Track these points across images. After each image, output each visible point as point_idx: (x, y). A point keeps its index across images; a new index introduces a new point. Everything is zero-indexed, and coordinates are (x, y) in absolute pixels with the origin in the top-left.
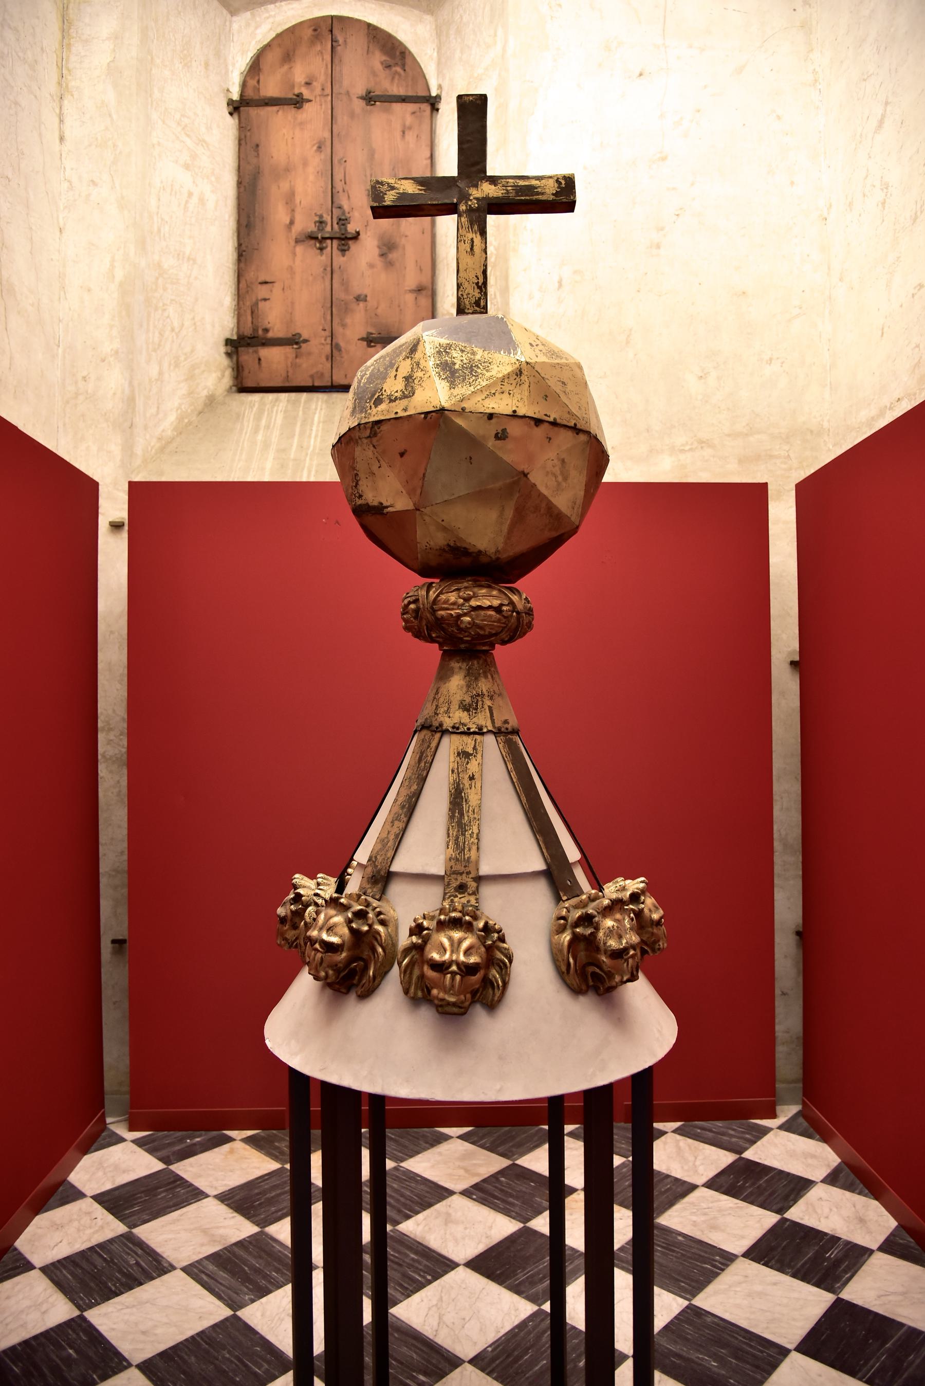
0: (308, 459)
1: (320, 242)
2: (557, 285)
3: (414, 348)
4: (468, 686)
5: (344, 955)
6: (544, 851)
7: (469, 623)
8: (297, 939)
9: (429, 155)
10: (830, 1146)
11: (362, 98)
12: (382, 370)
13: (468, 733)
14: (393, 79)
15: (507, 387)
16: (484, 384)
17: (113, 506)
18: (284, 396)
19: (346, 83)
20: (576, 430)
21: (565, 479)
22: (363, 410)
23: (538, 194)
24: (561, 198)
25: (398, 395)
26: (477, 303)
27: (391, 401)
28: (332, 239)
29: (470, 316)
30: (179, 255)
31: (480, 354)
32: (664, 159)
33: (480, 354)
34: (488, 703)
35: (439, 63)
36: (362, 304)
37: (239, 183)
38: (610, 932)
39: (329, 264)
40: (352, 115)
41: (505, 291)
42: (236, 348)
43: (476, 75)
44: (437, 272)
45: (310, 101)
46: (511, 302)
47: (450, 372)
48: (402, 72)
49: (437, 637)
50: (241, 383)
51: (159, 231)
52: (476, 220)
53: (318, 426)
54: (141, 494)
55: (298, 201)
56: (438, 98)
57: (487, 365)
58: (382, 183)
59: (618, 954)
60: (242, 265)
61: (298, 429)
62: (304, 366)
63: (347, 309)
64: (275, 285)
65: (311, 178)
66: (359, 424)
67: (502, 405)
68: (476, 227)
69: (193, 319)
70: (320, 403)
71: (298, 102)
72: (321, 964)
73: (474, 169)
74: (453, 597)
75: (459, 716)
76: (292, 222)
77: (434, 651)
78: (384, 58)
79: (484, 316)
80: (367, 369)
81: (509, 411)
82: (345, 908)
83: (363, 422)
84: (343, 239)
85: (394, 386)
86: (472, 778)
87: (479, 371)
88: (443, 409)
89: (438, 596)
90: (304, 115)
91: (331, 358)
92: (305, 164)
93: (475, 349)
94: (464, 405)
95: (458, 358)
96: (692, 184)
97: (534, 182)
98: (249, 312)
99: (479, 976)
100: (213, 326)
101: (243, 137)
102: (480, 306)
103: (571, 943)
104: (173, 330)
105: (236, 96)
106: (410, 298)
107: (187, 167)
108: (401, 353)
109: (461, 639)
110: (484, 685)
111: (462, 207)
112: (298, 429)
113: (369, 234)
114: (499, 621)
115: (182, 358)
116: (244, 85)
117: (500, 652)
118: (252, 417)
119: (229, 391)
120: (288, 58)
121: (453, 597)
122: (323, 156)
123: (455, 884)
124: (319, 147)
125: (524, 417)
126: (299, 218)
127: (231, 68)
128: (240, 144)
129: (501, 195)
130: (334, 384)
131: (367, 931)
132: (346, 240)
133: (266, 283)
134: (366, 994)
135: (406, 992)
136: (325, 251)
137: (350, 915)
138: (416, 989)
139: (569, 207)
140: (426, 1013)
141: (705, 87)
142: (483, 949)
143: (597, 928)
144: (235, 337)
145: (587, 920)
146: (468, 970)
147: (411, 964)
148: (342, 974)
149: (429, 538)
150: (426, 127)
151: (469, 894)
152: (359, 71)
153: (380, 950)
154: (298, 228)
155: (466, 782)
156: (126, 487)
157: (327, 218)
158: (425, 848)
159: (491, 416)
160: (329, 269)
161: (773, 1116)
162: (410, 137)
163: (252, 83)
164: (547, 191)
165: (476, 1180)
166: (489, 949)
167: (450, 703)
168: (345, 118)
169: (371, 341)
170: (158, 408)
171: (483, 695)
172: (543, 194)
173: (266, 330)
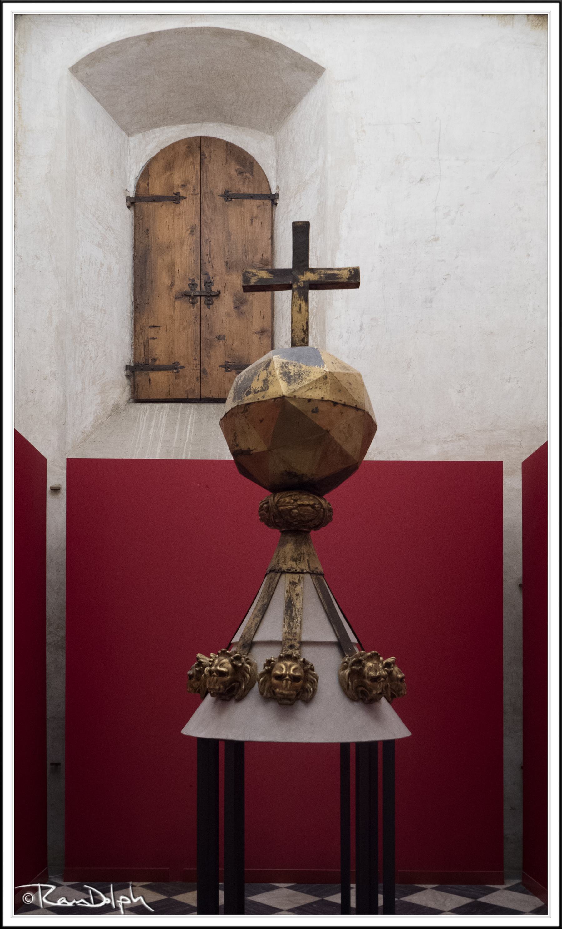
0: (185, 447)
1: (193, 298)
2: (359, 328)
3: (268, 364)
4: (296, 549)
5: (229, 677)
6: (337, 632)
7: (297, 513)
8: (199, 687)
9: (269, 237)
10: (538, 897)
11: (222, 196)
12: (250, 376)
13: (296, 573)
14: (244, 182)
15: (318, 385)
16: (306, 383)
17: (57, 476)
18: (166, 405)
19: (211, 185)
20: (357, 409)
21: (351, 435)
22: (240, 398)
23: (338, 278)
24: (352, 280)
25: (260, 389)
26: (303, 340)
27: (255, 393)
28: (201, 296)
29: (299, 348)
30: (94, 307)
31: (304, 368)
32: (436, 240)
33: (304, 368)
34: (307, 558)
35: (277, 171)
36: (221, 342)
37: (135, 257)
38: (371, 669)
39: (199, 314)
40: (215, 208)
41: (323, 333)
42: (133, 372)
43: (304, 181)
44: (275, 319)
45: (185, 198)
46: (327, 339)
47: (288, 377)
48: (251, 177)
49: (279, 522)
50: (137, 396)
51: (82, 291)
52: (302, 294)
53: (191, 426)
54: (76, 468)
55: (176, 270)
56: (277, 195)
57: (308, 373)
58: (249, 272)
59: (375, 679)
60: (137, 314)
61: (177, 428)
62: (181, 384)
63: (210, 345)
64: (161, 328)
65: (186, 253)
66: (238, 406)
67: (316, 394)
68: (303, 298)
69: (104, 351)
70: (192, 410)
71: (176, 199)
72: (216, 682)
73: (302, 264)
74: (288, 500)
75: (294, 564)
76: (172, 284)
77: (277, 533)
78: (238, 167)
79: (306, 347)
80: (241, 376)
81: (319, 397)
82: (229, 655)
83: (240, 404)
84: (209, 296)
85: (257, 384)
86: (297, 595)
87: (303, 376)
88: (284, 397)
89: (280, 499)
90: (181, 208)
91: (200, 379)
92: (182, 243)
93: (301, 365)
94: (295, 394)
95: (292, 369)
96: (456, 257)
97: (336, 272)
98: (142, 347)
99: (300, 683)
100: (118, 356)
101: (137, 223)
102: (305, 342)
103: (349, 674)
104: (91, 359)
105: (132, 195)
106: (256, 337)
107: (99, 246)
108: (261, 367)
109: (292, 523)
110: (304, 549)
111: (295, 286)
112: (177, 428)
113: (227, 292)
114: (313, 513)
115: (97, 378)
116: (138, 187)
117: (313, 533)
118: (145, 419)
119: (128, 401)
120: (169, 167)
121: (288, 500)
122: (194, 238)
123: (288, 645)
124: (192, 231)
125: (328, 401)
126: (177, 281)
127: (128, 174)
128: (135, 229)
129: (316, 279)
130: (202, 397)
131: (241, 666)
132: (211, 297)
133: (154, 327)
134: (240, 699)
135: (262, 694)
136: (195, 305)
137: (232, 658)
138: (267, 692)
139: (356, 285)
140: (272, 705)
141: (468, 188)
142: (302, 671)
143: (364, 666)
144: (132, 365)
145: (359, 662)
146: (295, 679)
147: (265, 681)
148: (227, 689)
149: (275, 467)
150: (268, 216)
151: (296, 650)
152: (220, 177)
153: (248, 675)
154: (177, 288)
155: (294, 597)
156: (64, 464)
157: (198, 281)
158: (272, 628)
159: (310, 400)
160: (199, 317)
161: (502, 883)
162: (256, 224)
163: (143, 185)
164: (344, 277)
165: (298, 905)
166: (306, 672)
167: (285, 557)
168: (210, 210)
169: (228, 368)
170: (82, 411)
171: (304, 554)
172: (341, 278)
173: (155, 360)
